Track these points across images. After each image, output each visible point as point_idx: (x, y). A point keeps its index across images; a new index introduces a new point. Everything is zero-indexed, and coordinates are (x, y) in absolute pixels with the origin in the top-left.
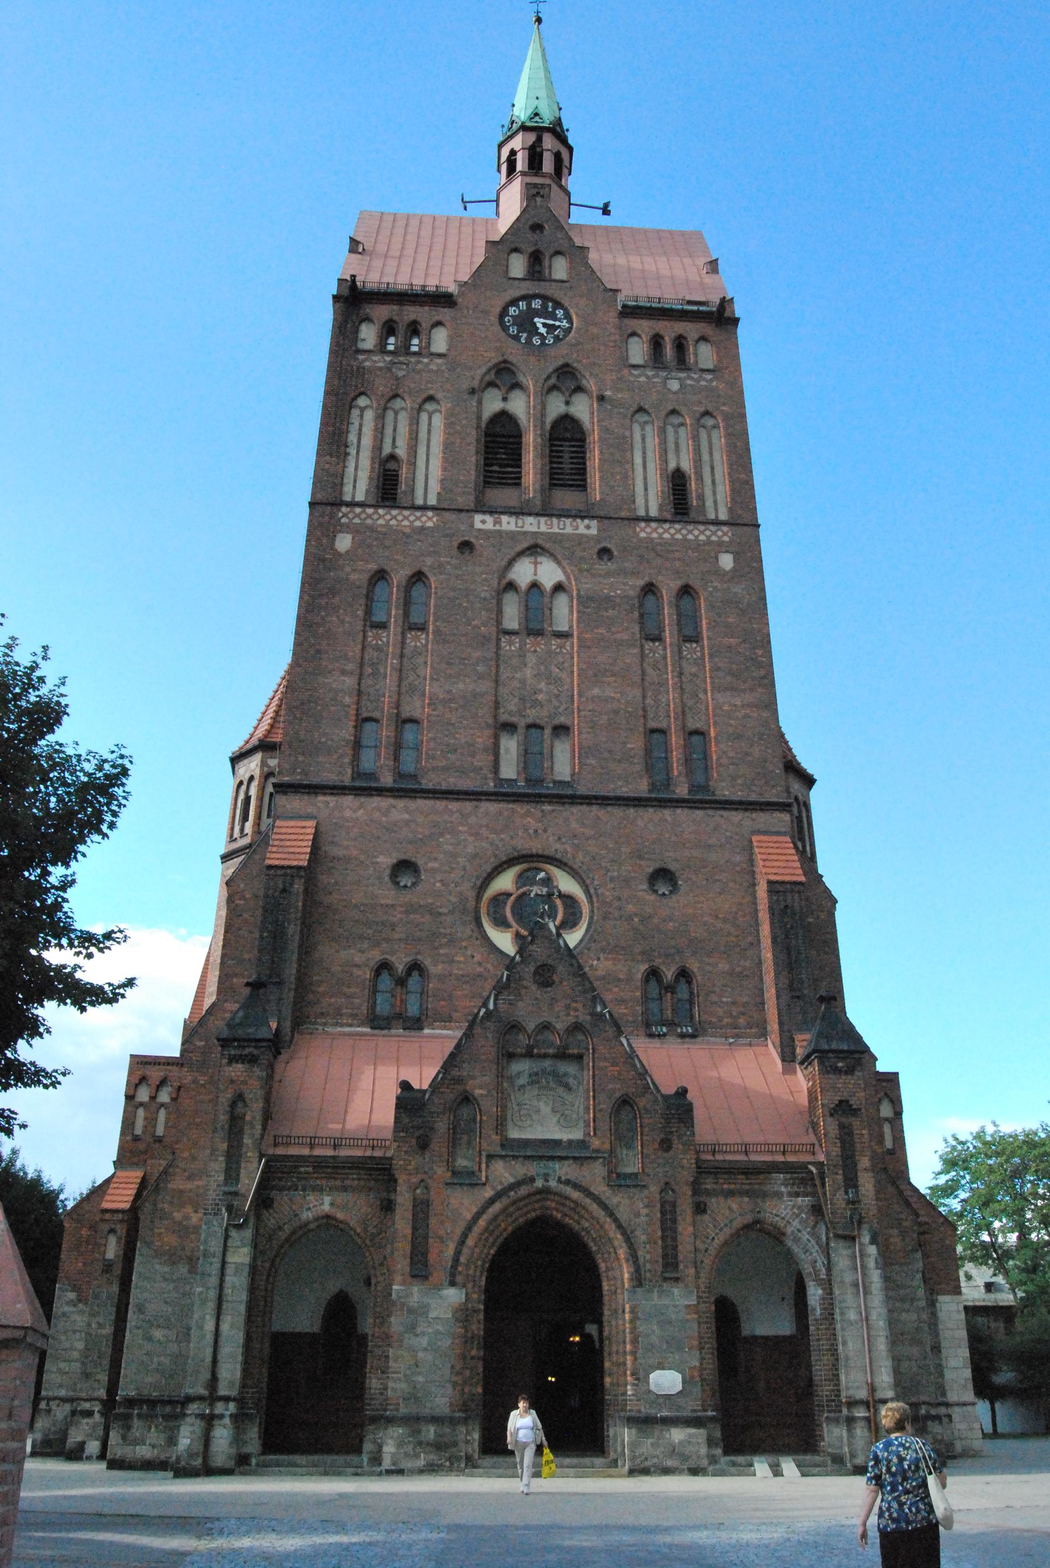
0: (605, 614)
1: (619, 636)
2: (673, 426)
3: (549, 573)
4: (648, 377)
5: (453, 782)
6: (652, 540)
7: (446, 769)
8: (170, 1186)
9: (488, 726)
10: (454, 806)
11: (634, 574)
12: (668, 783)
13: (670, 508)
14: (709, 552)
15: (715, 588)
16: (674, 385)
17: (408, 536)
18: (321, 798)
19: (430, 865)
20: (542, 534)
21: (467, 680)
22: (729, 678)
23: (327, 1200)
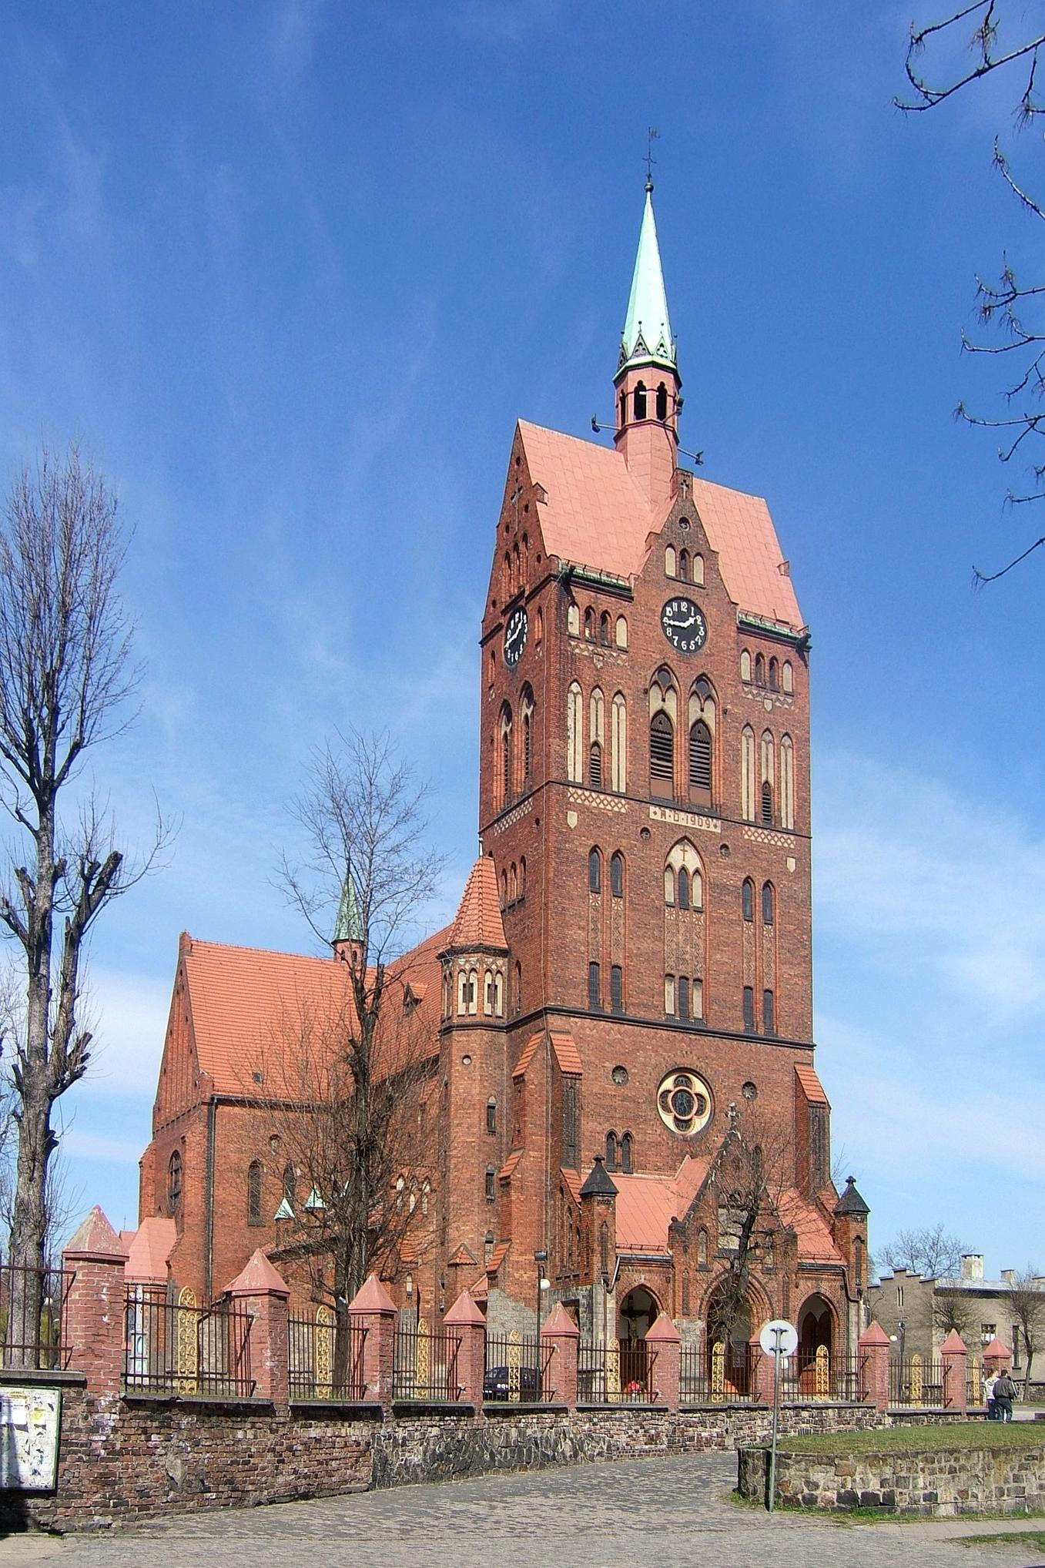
4: (753, 695)
5: (643, 1015)
7: (638, 1005)
10: (644, 1031)
14: (784, 853)
16: (768, 706)
19: (633, 1071)
20: (690, 828)
21: (649, 941)
22: (788, 954)
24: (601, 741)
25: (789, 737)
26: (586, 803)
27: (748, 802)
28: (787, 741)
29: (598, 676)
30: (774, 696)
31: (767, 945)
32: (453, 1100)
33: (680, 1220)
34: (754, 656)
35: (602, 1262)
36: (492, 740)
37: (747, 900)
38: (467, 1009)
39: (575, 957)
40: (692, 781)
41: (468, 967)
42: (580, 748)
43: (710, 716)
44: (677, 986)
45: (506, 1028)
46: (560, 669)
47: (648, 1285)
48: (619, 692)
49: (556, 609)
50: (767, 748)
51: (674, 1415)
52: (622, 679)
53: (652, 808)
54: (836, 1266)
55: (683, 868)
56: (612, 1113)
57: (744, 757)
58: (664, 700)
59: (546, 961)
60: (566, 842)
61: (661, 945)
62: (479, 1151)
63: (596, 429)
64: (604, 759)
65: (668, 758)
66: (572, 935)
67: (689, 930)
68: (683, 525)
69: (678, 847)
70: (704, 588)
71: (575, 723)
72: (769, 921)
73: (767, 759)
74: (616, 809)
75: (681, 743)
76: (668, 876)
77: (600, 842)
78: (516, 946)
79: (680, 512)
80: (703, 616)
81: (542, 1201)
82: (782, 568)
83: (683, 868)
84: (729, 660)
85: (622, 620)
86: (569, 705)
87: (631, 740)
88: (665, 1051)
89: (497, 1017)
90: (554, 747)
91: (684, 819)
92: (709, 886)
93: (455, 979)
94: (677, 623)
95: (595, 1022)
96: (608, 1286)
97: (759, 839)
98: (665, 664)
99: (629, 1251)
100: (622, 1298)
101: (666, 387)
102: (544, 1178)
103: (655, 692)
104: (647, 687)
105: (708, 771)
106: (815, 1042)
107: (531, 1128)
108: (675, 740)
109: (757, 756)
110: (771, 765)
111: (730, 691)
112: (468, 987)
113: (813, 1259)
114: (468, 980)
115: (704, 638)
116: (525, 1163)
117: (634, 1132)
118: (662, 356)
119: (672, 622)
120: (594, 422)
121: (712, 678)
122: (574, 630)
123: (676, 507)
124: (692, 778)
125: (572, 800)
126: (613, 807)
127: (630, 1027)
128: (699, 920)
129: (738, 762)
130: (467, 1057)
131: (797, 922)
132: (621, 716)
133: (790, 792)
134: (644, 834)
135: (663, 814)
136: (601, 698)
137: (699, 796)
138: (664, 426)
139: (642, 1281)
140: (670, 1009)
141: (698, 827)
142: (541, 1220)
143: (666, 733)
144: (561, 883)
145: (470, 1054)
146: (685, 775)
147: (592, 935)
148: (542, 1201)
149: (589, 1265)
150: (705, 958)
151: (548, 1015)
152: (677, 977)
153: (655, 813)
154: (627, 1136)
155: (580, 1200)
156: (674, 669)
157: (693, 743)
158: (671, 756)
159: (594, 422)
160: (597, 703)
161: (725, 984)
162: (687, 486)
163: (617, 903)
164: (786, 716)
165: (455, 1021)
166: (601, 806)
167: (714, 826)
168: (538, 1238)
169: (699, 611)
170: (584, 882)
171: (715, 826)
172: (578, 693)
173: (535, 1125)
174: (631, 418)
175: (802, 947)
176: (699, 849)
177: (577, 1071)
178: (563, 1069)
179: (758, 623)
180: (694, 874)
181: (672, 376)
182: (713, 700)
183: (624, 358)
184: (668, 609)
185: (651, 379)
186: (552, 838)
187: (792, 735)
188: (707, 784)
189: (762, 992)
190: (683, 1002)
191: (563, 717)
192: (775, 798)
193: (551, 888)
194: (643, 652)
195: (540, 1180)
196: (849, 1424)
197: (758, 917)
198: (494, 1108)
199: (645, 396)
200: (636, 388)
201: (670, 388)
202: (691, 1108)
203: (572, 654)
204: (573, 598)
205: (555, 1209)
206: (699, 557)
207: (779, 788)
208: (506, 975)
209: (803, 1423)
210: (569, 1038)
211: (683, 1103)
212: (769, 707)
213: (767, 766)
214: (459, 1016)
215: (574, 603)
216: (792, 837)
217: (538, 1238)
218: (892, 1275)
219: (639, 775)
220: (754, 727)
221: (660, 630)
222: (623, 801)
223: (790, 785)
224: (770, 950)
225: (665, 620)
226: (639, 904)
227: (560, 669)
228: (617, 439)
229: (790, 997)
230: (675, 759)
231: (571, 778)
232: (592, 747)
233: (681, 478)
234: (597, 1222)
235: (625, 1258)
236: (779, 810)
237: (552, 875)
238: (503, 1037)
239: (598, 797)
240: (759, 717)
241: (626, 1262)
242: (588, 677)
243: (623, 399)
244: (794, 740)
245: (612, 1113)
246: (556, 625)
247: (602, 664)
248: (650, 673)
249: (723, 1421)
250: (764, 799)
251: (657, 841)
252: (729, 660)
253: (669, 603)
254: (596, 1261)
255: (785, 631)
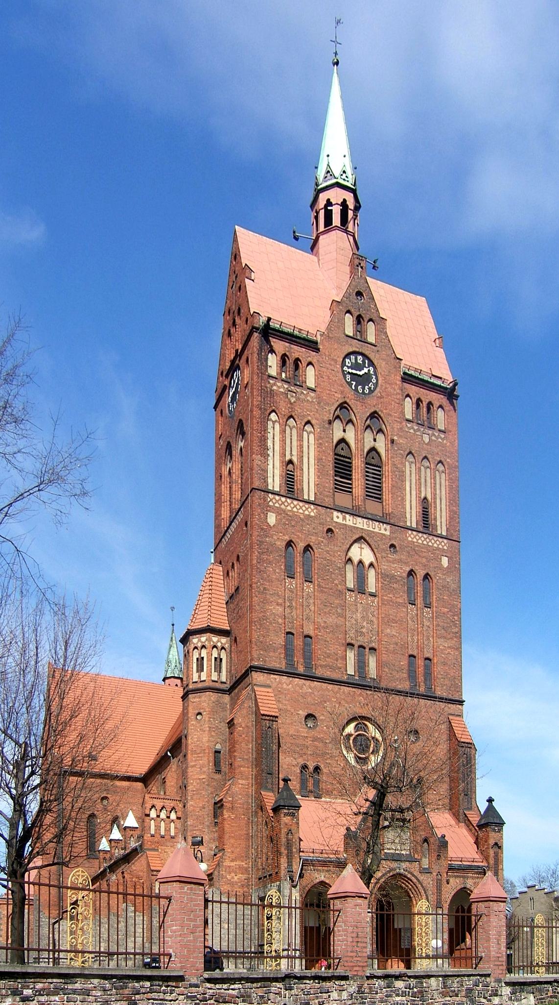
0: (392, 586)
1: (398, 600)
2: (409, 462)
3: (368, 556)
4: (414, 430)
5: (328, 674)
6: (414, 542)
7: (326, 666)
8: (224, 864)
9: (343, 644)
10: (330, 687)
11: (406, 563)
12: (416, 686)
13: (284, 488)
14: (437, 554)
15: (440, 577)
16: (426, 439)
17: (302, 520)
18: (272, 676)
19: (321, 718)
20: (365, 530)
21: (333, 617)
22: (443, 631)
23: (323, 875)
24: (295, 459)
25: (442, 463)
26: (283, 506)
27: (411, 512)
28: (440, 467)
29: (292, 408)
30: (430, 432)
31: (426, 623)
32: (190, 747)
33: (353, 829)
34: (414, 400)
35: (288, 862)
36: (221, 476)
37: (410, 590)
38: (200, 676)
39: (274, 627)
40: (367, 495)
41: (199, 645)
42: (277, 464)
43: (381, 445)
44: (356, 653)
45: (228, 691)
46: (261, 401)
47: (327, 882)
48: (308, 422)
49: (258, 354)
50: (426, 472)
51: (197, 986)
52: (311, 411)
53: (335, 514)
54: (478, 867)
55: (361, 562)
56: (305, 750)
57: (408, 478)
58: (344, 431)
59: (251, 629)
60: (267, 536)
61: (343, 620)
62: (207, 785)
63: (296, 238)
64: (297, 473)
65: (349, 477)
66: (271, 610)
67: (365, 610)
68: (359, 297)
69: (356, 545)
70: (376, 346)
71: (274, 445)
72: (428, 606)
73: (426, 480)
74: (307, 513)
75: (358, 465)
76: (349, 567)
77: (293, 537)
78: (234, 626)
79: (356, 286)
80: (375, 368)
81: (249, 819)
82: (437, 341)
83: (361, 562)
84: (395, 402)
85: (310, 367)
86: (269, 431)
87: (319, 460)
88: (347, 702)
89: (222, 683)
90: (256, 462)
91: (361, 523)
92: (383, 577)
93: (191, 654)
94: (354, 372)
95: (291, 679)
96: (293, 881)
97: (420, 541)
98: (345, 402)
99: (312, 855)
100: (306, 892)
101: (348, 203)
102: (250, 801)
103: (337, 425)
104: (331, 419)
105: (380, 489)
106: (464, 699)
107: (240, 761)
108: (354, 462)
109: (417, 477)
110: (429, 484)
111: (397, 426)
112: (200, 660)
113: (461, 861)
114: (200, 654)
115: (376, 385)
116: (235, 789)
117: (322, 766)
118: (344, 180)
119: (350, 371)
120: (294, 232)
121: (382, 415)
122: (273, 371)
123: (353, 283)
124: (367, 493)
125: (271, 503)
126: (304, 511)
127: (319, 683)
128: (373, 602)
129: (403, 481)
130: (199, 714)
131: (449, 606)
132: (310, 440)
133: (444, 507)
134: (329, 534)
135: (344, 518)
136: (294, 427)
137: (372, 507)
138: (346, 231)
139: (322, 878)
140: (351, 671)
141: (372, 530)
142: (248, 834)
143: (346, 457)
144: (262, 568)
145: (201, 711)
146: (361, 489)
147: (288, 611)
148: (249, 819)
149: (278, 866)
150: (378, 631)
151: (253, 673)
152: (356, 646)
153: (338, 517)
154: (317, 769)
155: (272, 815)
156: (352, 406)
157: (369, 466)
158: (351, 475)
159: (294, 232)
160: (291, 430)
161: (394, 652)
162: (362, 267)
163: (308, 587)
164: (440, 448)
165: (191, 687)
166: (295, 509)
167: (384, 530)
168: (245, 848)
169: (371, 363)
170: (281, 569)
171: (386, 530)
172: (276, 421)
173: (243, 759)
174: (322, 228)
175: (454, 625)
176: (373, 546)
177: (273, 714)
178: (262, 712)
179: (417, 375)
180: (369, 567)
181: (352, 195)
182: (383, 433)
183: (317, 185)
184: (347, 361)
185: (336, 196)
186: (255, 533)
187: (445, 463)
188: (380, 499)
189: (423, 659)
190: (361, 665)
191: (264, 439)
192: (432, 510)
193: (254, 572)
194: (328, 392)
195: (247, 802)
196: (457, 995)
197: (420, 601)
198: (219, 752)
199: (332, 210)
200: (325, 205)
201: (351, 204)
202: (368, 747)
203: (271, 390)
204: (271, 346)
205: (258, 825)
206: (371, 323)
207: (435, 503)
208: (228, 650)
209: (398, 995)
210: (269, 690)
211: (362, 745)
212: (427, 440)
213: (426, 486)
214: (193, 683)
215: (272, 351)
216: (445, 541)
217: (245, 848)
218: (526, 889)
219: (324, 487)
220: (415, 455)
221: (340, 375)
222: (312, 507)
223: (444, 502)
224: (429, 627)
225: (345, 368)
226: (325, 588)
227: (261, 401)
228: (312, 248)
229: (445, 664)
230: (354, 477)
231: (270, 487)
232: (287, 465)
233: (357, 262)
234: (284, 831)
235: (307, 860)
236: (435, 519)
237: (255, 562)
238: (226, 698)
239: (292, 502)
240: (419, 447)
241: (306, 863)
242: (284, 409)
243: (316, 218)
244: (446, 467)
245: (305, 750)
246: (258, 366)
247: (294, 399)
248: (334, 408)
249: (279, 994)
250: (423, 511)
251: (339, 539)
252: (395, 402)
253: (348, 355)
254: (283, 861)
255: (438, 382)
